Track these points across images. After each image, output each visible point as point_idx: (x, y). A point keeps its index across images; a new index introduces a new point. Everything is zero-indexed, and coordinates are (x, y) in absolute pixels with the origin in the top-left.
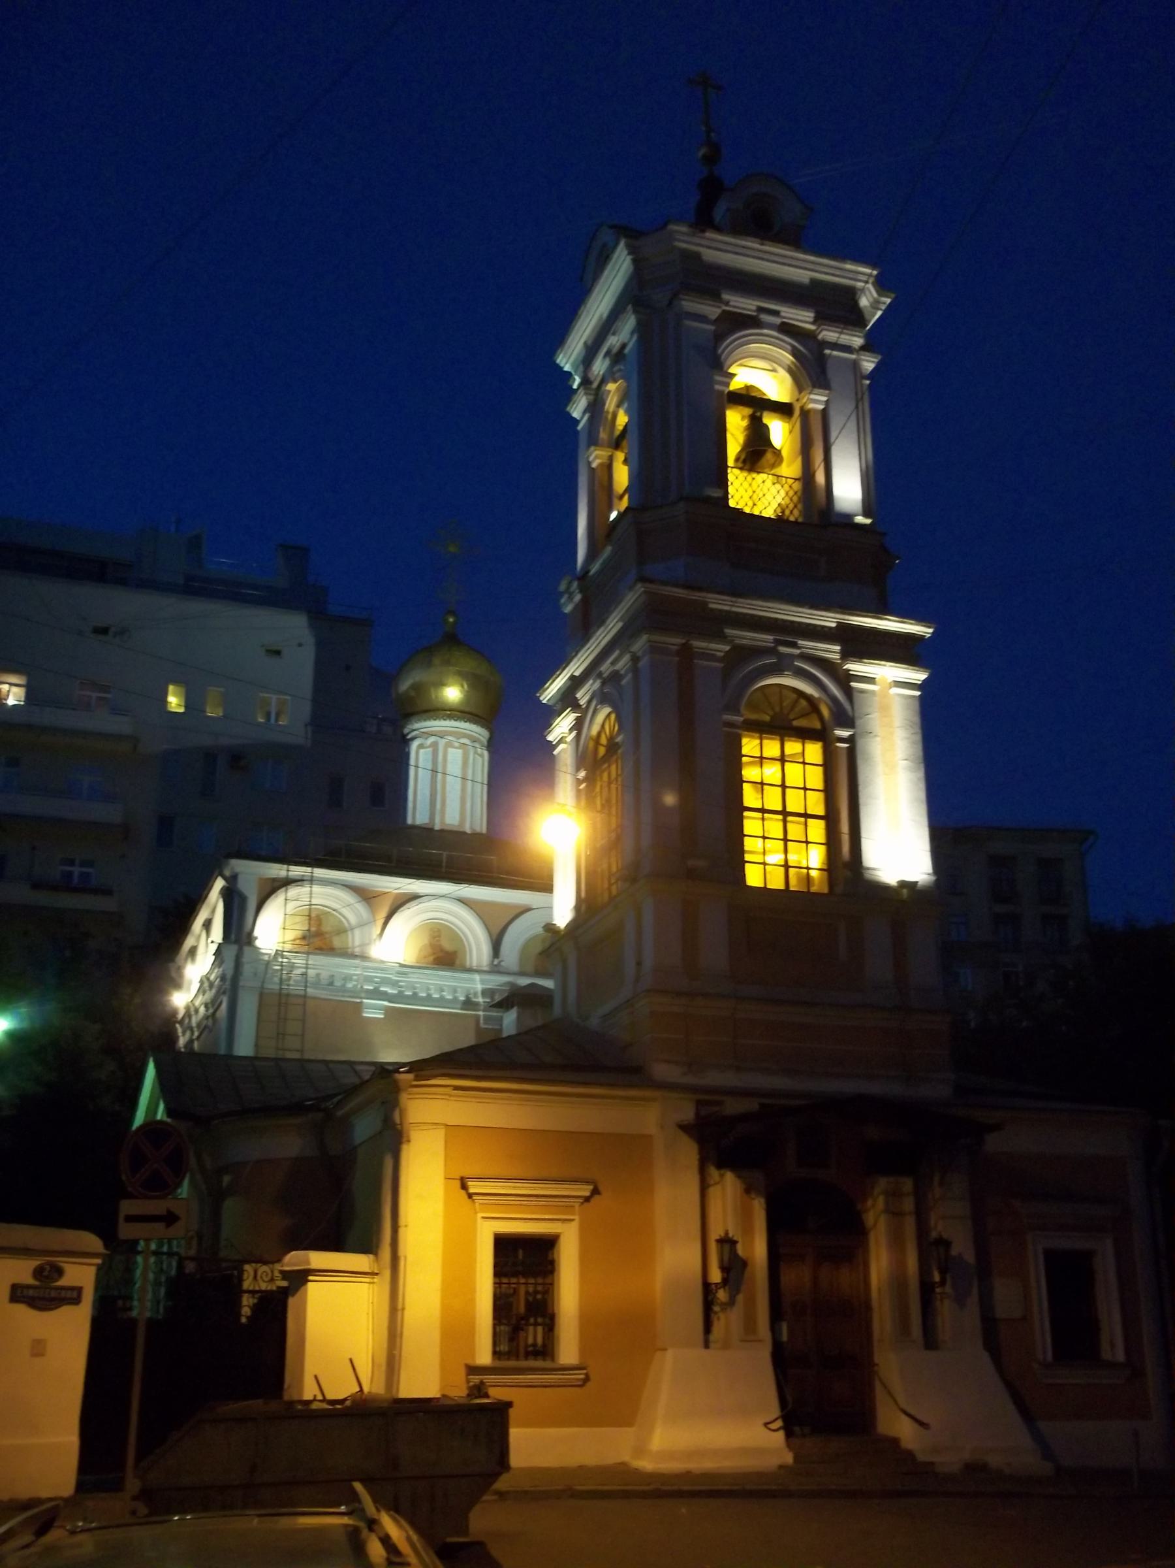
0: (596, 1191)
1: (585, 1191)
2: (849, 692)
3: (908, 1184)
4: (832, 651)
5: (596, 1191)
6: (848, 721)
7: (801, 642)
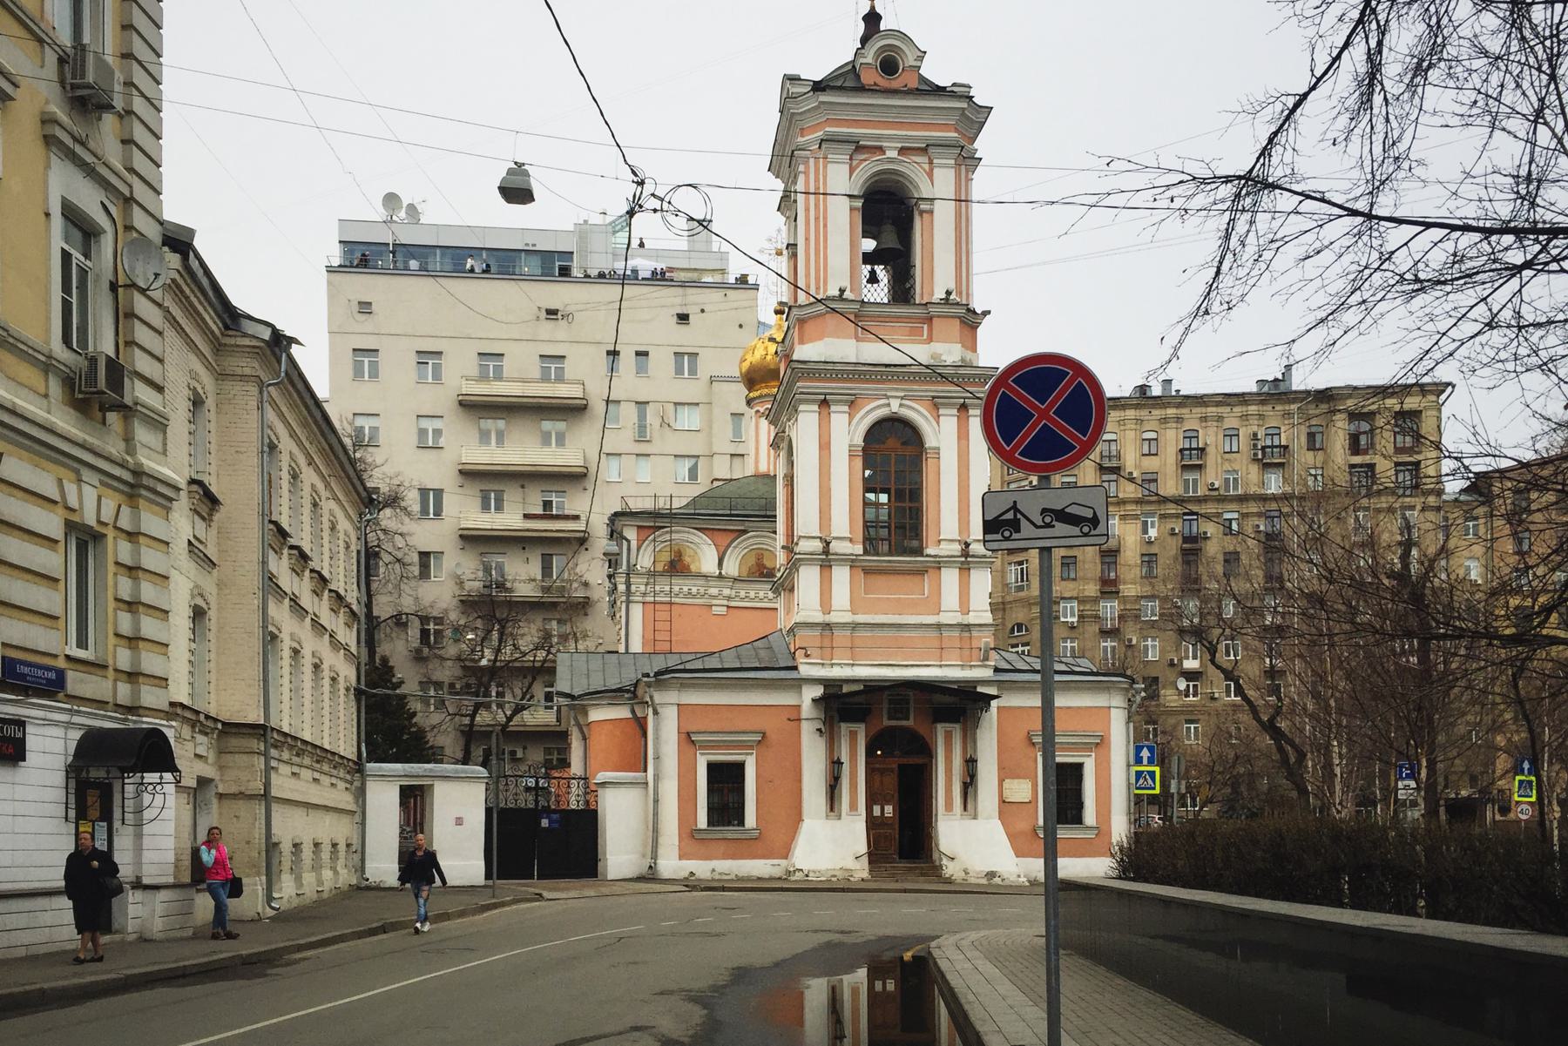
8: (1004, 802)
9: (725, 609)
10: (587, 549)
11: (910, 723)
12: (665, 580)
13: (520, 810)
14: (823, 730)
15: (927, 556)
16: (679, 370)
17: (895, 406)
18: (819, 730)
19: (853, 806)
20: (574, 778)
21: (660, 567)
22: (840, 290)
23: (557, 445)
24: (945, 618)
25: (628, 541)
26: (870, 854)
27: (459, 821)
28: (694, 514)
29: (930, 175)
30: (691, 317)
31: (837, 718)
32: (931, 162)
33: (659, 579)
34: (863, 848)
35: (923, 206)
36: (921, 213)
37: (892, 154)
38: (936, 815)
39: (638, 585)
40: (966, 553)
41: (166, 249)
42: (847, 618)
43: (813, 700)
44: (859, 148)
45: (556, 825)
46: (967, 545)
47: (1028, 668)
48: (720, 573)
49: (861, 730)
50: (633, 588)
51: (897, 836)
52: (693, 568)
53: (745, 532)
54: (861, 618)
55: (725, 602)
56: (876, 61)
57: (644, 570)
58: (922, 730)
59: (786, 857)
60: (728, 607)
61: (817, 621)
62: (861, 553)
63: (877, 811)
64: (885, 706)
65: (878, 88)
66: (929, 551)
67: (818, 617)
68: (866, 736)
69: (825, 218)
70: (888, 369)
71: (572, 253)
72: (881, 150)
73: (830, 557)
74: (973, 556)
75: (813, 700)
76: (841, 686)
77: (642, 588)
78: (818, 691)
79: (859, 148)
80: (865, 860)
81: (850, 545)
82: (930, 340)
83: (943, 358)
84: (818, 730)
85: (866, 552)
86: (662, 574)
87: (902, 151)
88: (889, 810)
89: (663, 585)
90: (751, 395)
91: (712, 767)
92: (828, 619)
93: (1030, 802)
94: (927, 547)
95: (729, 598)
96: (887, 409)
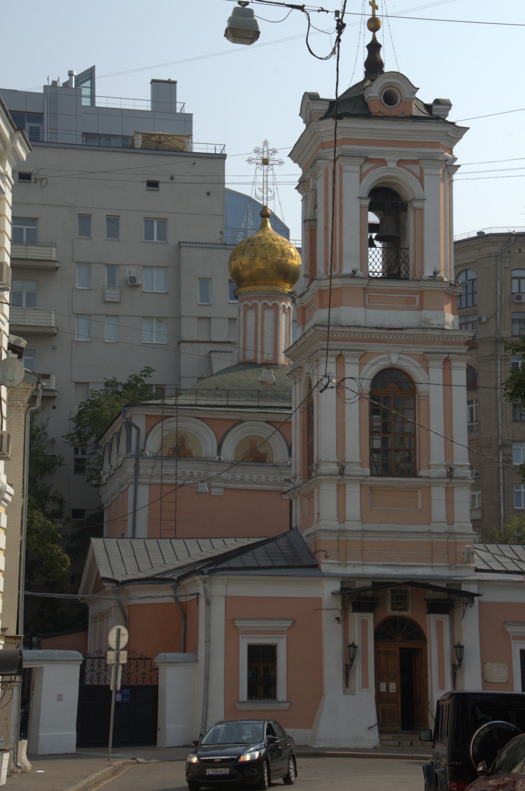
1: (289, 624)
3: (445, 618)
8: (486, 681)
9: (222, 490)
10: (54, 407)
11: (408, 614)
12: (172, 463)
13: (95, 686)
14: (341, 618)
15: (420, 477)
16: (149, 236)
17: (394, 360)
18: (338, 619)
19: (365, 685)
20: (141, 659)
21: (165, 454)
22: (353, 271)
23: (27, 306)
24: (435, 528)
25: (138, 430)
26: (379, 724)
27: (60, 698)
28: (196, 405)
29: (421, 180)
30: (160, 185)
31: (350, 608)
32: (421, 170)
33: (165, 463)
34: (372, 718)
35: (416, 205)
36: (415, 209)
37: (392, 165)
38: (432, 692)
39: (145, 467)
40: (450, 475)
41: (10, 352)
42: (359, 526)
43: (332, 593)
44: (367, 160)
45: (126, 699)
46: (452, 470)
47: (501, 568)
48: (220, 459)
49: (370, 617)
50: (141, 471)
51: (400, 710)
52: (194, 453)
53: (240, 422)
54: (368, 527)
55: (223, 485)
56: (380, 95)
57: (151, 455)
58: (418, 620)
59: (310, 726)
60: (225, 489)
61: (334, 529)
62: (369, 474)
63: (383, 687)
64: (389, 598)
65: (382, 115)
66: (422, 473)
67: (336, 525)
68: (374, 624)
69: (341, 213)
70: (389, 332)
71: (43, 114)
72: (383, 162)
73: (344, 477)
74: (456, 478)
75: (332, 593)
76: (354, 582)
77: (149, 471)
78: (336, 586)
79: (367, 160)
80: (376, 730)
81: (360, 468)
82: (421, 308)
83: (432, 322)
84: (338, 619)
85: (372, 475)
86: (168, 458)
87: (400, 163)
88: (393, 687)
89: (169, 467)
90: (74, 77)
91: (251, 648)
92: (342, 526)
93: (507, 682)
94: (420, 470)
95: (226, 481)
96: (389, 361)
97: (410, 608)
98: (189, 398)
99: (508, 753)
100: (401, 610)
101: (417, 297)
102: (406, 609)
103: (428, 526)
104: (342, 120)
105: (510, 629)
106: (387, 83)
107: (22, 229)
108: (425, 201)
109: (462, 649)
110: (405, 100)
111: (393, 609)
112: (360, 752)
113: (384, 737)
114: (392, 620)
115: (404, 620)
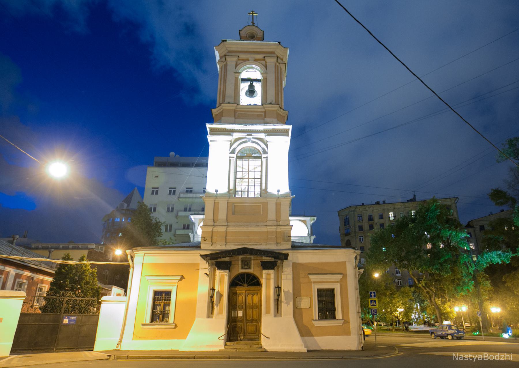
0: (182, 277)
1: (179, 278)
2: (267, 147)
3: (272, 272)
4: (262, 136)
5: (182, 277)
6: (265, 152)
7: (253, 134)
19: (220, 312)
97: (252, 266)
98: (252, 289)
99: (218, 255)
100: (246, 269)
101: (263, 114)
102: (250, 268)
103: (265, 223)
104: (300, 337)
105: (312, 277)
106: (253, 32)
107: (171, 190)
108: (268, 74)
109: (279, 289)
110: (264, 70)
111: (242, 268)
112: (157, 360)
113: (228, 343)
114: (242, 275)
115: (249, 275)
